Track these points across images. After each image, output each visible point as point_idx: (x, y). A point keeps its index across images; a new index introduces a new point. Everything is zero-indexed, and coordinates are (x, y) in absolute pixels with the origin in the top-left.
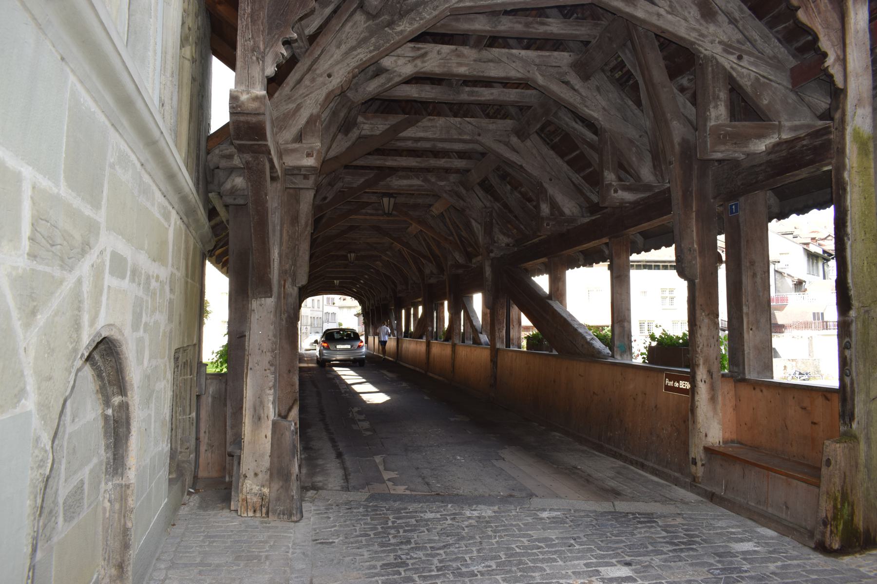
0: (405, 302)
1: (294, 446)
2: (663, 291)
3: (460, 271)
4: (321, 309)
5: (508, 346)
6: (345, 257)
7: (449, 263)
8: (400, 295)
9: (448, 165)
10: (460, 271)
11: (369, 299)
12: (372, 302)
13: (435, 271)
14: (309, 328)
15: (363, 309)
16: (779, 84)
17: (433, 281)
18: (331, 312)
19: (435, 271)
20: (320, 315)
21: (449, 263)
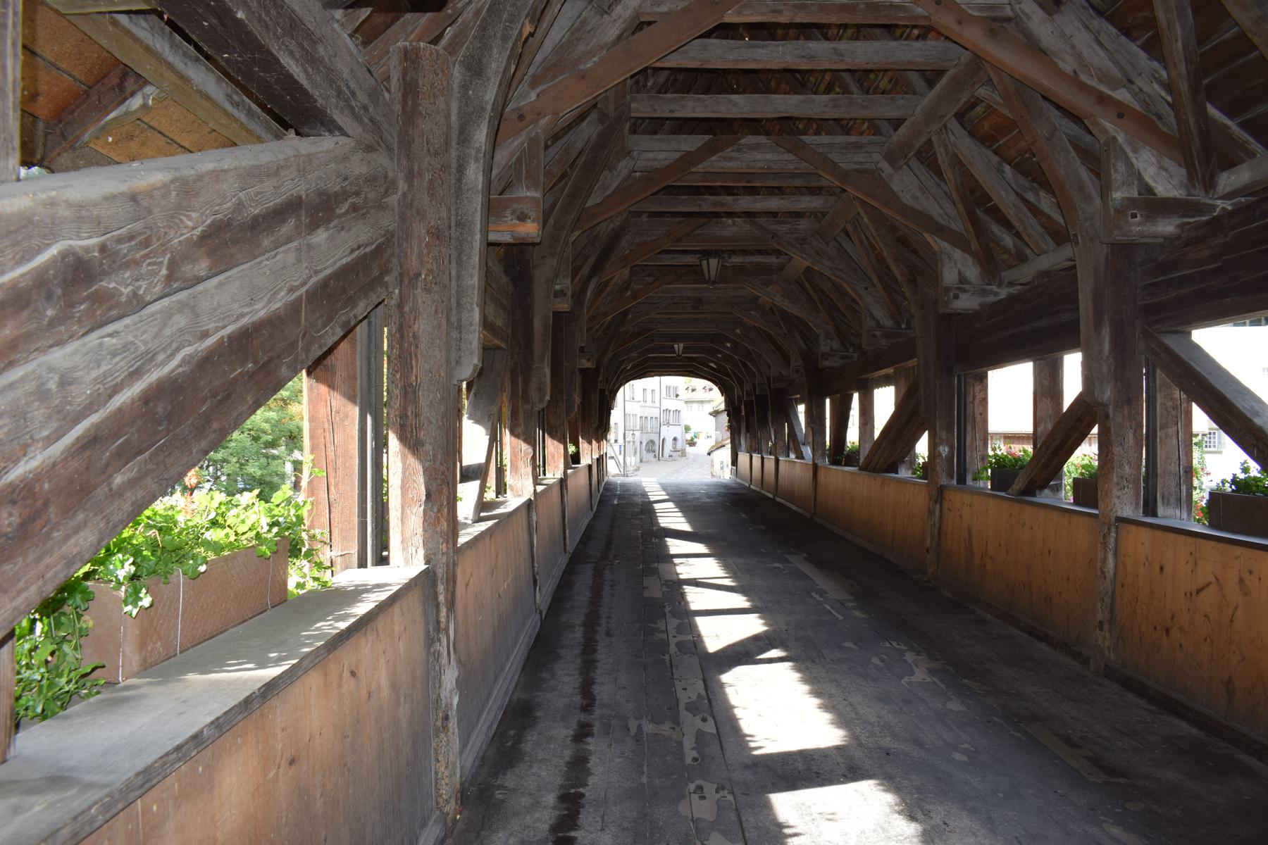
8: (827, 363)
11: (740, 382)
14: (637, 434)
17: (967, 303)
20: (656, 413)
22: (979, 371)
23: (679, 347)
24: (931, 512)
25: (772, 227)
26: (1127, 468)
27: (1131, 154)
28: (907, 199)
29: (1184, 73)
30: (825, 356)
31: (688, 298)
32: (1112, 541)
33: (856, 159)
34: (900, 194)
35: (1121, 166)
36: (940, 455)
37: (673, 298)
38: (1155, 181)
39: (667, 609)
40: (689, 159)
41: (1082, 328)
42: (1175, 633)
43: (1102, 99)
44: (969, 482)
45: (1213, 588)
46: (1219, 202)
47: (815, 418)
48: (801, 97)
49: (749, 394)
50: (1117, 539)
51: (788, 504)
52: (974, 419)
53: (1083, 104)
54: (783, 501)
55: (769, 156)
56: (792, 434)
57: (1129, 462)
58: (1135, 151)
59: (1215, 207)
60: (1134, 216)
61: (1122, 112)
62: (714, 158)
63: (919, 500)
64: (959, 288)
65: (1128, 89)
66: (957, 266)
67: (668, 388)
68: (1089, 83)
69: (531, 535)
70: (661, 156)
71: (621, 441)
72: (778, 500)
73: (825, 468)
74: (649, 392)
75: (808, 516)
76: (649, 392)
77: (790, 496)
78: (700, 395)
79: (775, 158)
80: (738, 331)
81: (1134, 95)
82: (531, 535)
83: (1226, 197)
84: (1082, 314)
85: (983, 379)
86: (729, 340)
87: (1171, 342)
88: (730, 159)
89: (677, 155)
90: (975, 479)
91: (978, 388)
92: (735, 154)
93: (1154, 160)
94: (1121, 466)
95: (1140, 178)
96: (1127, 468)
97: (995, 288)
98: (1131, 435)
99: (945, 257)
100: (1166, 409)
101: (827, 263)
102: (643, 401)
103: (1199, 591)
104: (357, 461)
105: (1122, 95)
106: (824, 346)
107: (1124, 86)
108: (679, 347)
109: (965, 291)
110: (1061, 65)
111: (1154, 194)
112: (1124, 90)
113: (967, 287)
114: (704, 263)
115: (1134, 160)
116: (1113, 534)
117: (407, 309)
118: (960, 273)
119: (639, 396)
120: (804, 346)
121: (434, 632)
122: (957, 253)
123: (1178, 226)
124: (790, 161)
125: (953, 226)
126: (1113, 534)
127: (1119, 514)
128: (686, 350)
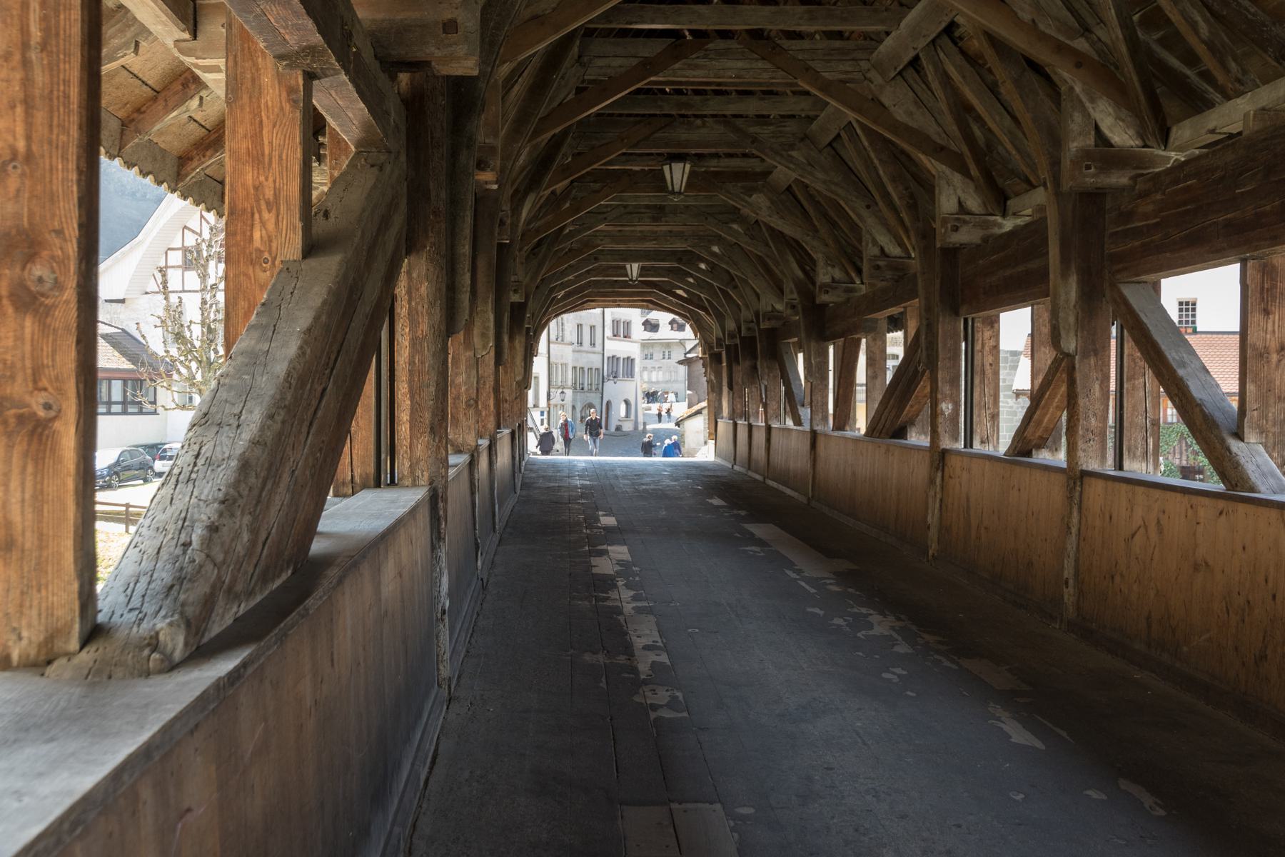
0: (830, 324)
1: (282, 109)
2: (1181, 304)
3: (1119, 179)
4: (598, 348)
5: (969, 443)
6: (658, 181)
7: (1074, 146)
8: (824, 298)
9: (406, 372)
10: (1119, 179)
11: (720, 318)
12: (731, 325)
13: (973, 203)
14: (569, 393)
15: (706, 344)
16: (311, 424)
17: (967, 236)
18: (622, 355)
19: (973, 203)
20: (595, 361)
21: (1074, 146)
22: (992, 312)
23: (634, 269)
24: (932, 481)
25: (752, 130)
26: (1093, 420)
27: (1088, 104)
28: (900, 114)
29: (1121, 36)
30: (826, 288)
31: (647, 207)
32: (1077, 494)
33: (841, 67)
34: (892, 109)
35: (1077, 117)
36: (943, 413)
37: (625, 207)
38: (1112, 131)
39: (620, 583)
40: (648, 66)
41: (1051, 276)
42: (1118, 579)
43: (1060, 48)
44: (977, 446)
45: (1142, 530)
46: (1173, 154)
47: (816, 370)
48: (773, 8)
49: (732, 336)
50: (1081, 493)
51: (781, 488)
52: (983, 372)
53: (1043, 55)
54: (775, 484)
55: (740, 64)
56: (789, 394)
57: (1095, 415)
58: (1092, 100)
59: (1169, 158)
60: (1088, 167)
61: (1080, 61)
62: (677, 66)
63: (920, 470)
64: (958, 219)
65: (1087, 39)
66: (954, 194)
67: (616, 323)
68: (1048, 31)
69: (473, 494)
70: (617, 62)
71: (543, 403)
72: (770, 483)
73: (826, 435)
74: (586, 331)
75: (803, 499)
76: (586, 331)
77: (784, 477)
78: (665, 333)
79: (748, 66)
80: (716, 249)
81: (1092, 44)
82: (473, 494)
83: (1180, 149)
84: (1051, 261)
85: (994, 323)
86: (702, 260)
87: (1129, 292)
88: (696, 67)
89: (634, 62)
90: (982, 442)
91: (987, 334)
92: (701, 62)
93: (1111, 110)
94: (1087, 418)
95: (1097, 128)
96: (1093, 420)
97: (999, 219)
98: (1097, 387)
99: (943, 183)
100: (1134, 360)
101: (820, 175)
102: (572, 343)
103: (1133, 536)
104: (374, 400)
105: (1081, 44)
106: (823, 276)
107: (1082, 35)
108: (634, 269)
109: (965, 222)
110: (1020, 14)
111: (1111, 145)
112: (1082, 40)
113: (967, 217)
114: (666, 168)
115: (1091, 110)
116: (1078, 489)
117: (414, 275)
118: (960, 203)
119: (571, 335)
120: (799, 273)
121: (437, 535)
122: (957, 178)
123: (1131, 178)
124: (765, 70)
125: (953, 147)
126: (1078, 489)
127: (1084, 467)
128: (643, 272)
